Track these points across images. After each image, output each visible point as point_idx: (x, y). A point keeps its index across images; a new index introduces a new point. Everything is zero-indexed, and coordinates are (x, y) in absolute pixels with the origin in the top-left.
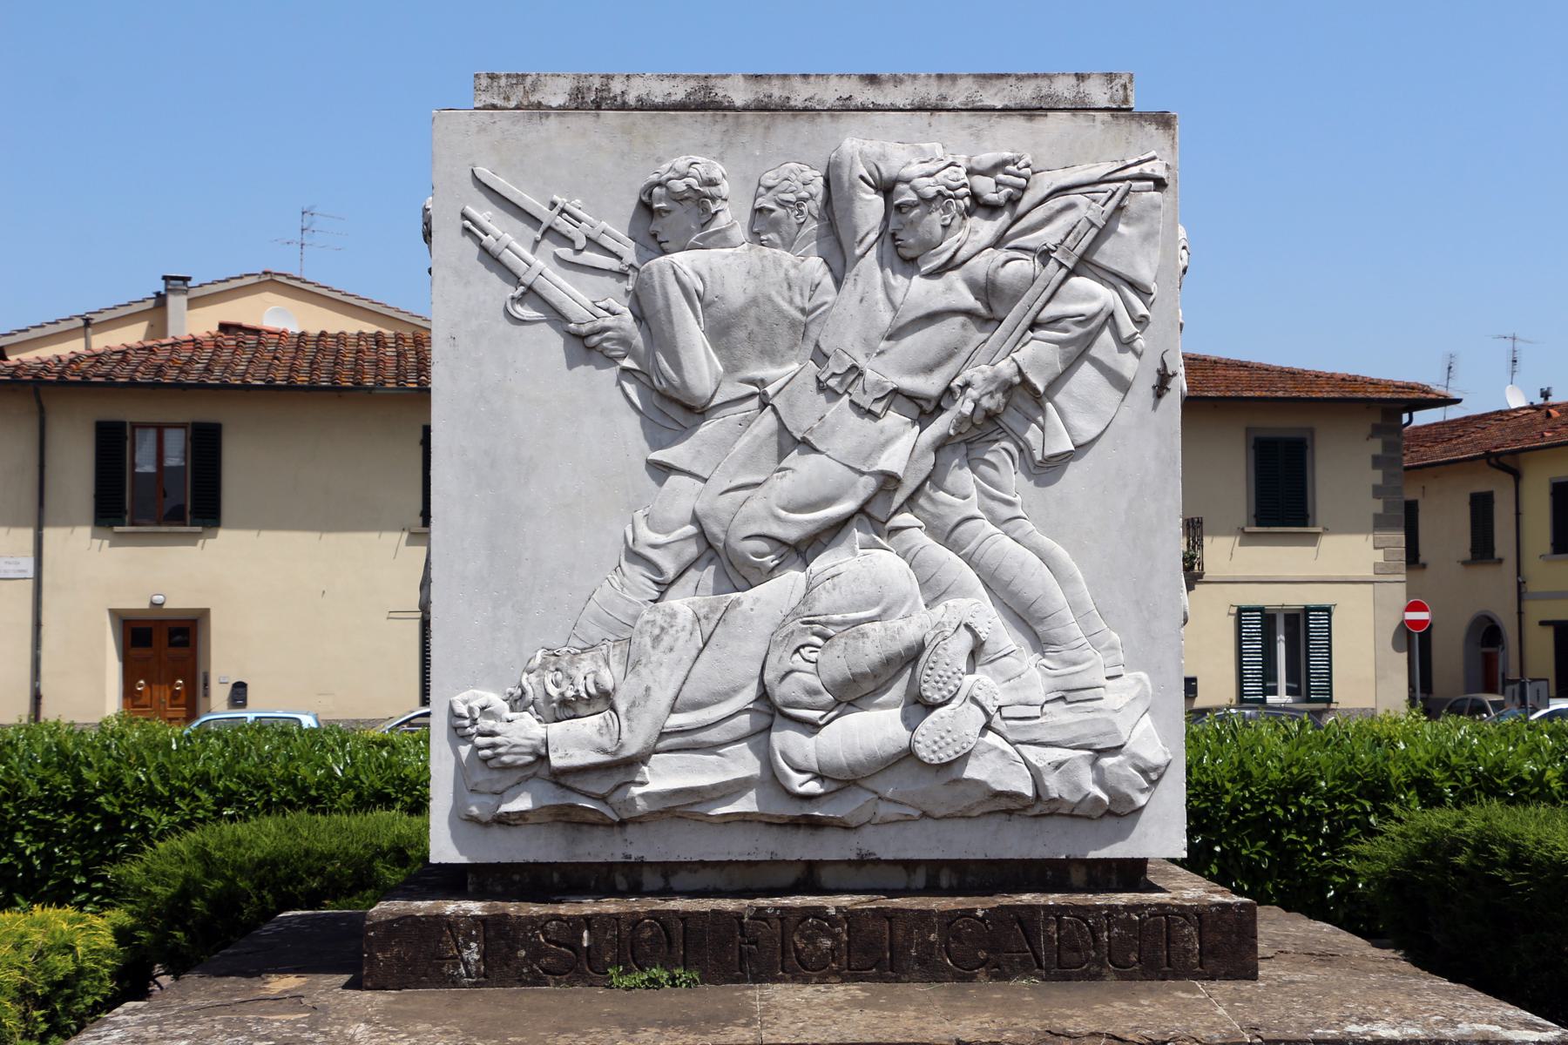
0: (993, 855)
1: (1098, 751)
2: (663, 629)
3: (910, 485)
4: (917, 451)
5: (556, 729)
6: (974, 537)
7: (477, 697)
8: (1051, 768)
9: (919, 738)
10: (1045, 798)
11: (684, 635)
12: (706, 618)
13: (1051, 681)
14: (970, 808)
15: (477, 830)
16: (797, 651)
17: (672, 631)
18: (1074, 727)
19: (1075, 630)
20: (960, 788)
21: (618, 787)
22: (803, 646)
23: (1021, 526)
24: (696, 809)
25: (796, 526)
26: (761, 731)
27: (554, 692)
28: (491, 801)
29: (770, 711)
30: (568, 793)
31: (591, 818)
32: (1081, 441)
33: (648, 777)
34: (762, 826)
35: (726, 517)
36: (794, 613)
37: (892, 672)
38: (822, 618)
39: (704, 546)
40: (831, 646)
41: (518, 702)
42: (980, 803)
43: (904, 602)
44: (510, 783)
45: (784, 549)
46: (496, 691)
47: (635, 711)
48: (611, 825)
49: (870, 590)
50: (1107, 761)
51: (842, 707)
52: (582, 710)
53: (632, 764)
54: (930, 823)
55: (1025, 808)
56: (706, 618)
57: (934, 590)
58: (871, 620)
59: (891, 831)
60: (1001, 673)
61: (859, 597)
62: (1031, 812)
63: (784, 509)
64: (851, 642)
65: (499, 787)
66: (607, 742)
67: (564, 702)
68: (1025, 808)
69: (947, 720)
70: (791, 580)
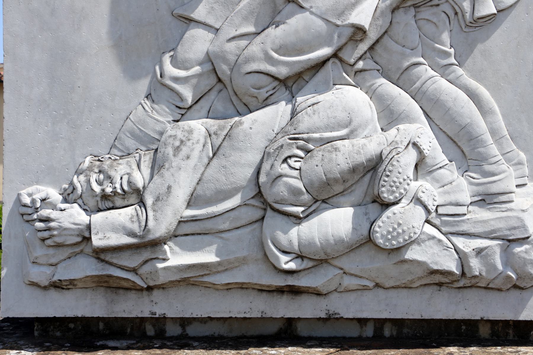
0: (426, 316)
1: (509, 241)
2: (182, 142)
3: (373, 36)
4: (378, 11)
5: (98, 218)
6: (419, 78)
7: (39, 191)
8: (474, 253)
9: (377, 229)
10: (468, 275)
11: (199, 147)
12: (216, 134)
13: (475, 188)
14: (412, 281)
15: (38, 292)
16: (285, 161)
17: (189, 143)
18: (492, 223)
19: (494, 150)
20: (406, 266)
21: (146, 262)
22: (290, 157)
23: (454, 71)
24: (206, 279)
25: (285, 65)
26: (256, 221)
27: (97, 189)
28: (48, 271)
29: (263, 203)
30: (107, 266)
31: (125, 284)
32: (502, 6)
33: (169, 254)
34: (255, 293)
35: (232, 58)
36: (283, 131)
37: (356, 178)
38: (305, 136)
39: (215, 80)
40: (311, 157)
41: (69, 196)
42: (419, 278)
43: (366, 126)
44: (62, 258)
45: (276, 83)
46: (54, 187)
47: (159, 204)
48: (141, 289)
49: (342, 116)
50: (518, 249)
51: (318, 204)
52: (119, 202)
53: (156, 244)
54: (381, 291)
55: (452, 282)
56: (216, 134)
57: (390, 117)
58: (342, 138)
59: (352, 297)
60: (437, 181)
61: (333, 121)
62: (456, 285)
63: (276, 52)
64: (326, 154)
65: (53, 261)
66: (135, 227)
67: (105, 197)
68: (452, 282)
69: (398, 215)
70: (281, 110)
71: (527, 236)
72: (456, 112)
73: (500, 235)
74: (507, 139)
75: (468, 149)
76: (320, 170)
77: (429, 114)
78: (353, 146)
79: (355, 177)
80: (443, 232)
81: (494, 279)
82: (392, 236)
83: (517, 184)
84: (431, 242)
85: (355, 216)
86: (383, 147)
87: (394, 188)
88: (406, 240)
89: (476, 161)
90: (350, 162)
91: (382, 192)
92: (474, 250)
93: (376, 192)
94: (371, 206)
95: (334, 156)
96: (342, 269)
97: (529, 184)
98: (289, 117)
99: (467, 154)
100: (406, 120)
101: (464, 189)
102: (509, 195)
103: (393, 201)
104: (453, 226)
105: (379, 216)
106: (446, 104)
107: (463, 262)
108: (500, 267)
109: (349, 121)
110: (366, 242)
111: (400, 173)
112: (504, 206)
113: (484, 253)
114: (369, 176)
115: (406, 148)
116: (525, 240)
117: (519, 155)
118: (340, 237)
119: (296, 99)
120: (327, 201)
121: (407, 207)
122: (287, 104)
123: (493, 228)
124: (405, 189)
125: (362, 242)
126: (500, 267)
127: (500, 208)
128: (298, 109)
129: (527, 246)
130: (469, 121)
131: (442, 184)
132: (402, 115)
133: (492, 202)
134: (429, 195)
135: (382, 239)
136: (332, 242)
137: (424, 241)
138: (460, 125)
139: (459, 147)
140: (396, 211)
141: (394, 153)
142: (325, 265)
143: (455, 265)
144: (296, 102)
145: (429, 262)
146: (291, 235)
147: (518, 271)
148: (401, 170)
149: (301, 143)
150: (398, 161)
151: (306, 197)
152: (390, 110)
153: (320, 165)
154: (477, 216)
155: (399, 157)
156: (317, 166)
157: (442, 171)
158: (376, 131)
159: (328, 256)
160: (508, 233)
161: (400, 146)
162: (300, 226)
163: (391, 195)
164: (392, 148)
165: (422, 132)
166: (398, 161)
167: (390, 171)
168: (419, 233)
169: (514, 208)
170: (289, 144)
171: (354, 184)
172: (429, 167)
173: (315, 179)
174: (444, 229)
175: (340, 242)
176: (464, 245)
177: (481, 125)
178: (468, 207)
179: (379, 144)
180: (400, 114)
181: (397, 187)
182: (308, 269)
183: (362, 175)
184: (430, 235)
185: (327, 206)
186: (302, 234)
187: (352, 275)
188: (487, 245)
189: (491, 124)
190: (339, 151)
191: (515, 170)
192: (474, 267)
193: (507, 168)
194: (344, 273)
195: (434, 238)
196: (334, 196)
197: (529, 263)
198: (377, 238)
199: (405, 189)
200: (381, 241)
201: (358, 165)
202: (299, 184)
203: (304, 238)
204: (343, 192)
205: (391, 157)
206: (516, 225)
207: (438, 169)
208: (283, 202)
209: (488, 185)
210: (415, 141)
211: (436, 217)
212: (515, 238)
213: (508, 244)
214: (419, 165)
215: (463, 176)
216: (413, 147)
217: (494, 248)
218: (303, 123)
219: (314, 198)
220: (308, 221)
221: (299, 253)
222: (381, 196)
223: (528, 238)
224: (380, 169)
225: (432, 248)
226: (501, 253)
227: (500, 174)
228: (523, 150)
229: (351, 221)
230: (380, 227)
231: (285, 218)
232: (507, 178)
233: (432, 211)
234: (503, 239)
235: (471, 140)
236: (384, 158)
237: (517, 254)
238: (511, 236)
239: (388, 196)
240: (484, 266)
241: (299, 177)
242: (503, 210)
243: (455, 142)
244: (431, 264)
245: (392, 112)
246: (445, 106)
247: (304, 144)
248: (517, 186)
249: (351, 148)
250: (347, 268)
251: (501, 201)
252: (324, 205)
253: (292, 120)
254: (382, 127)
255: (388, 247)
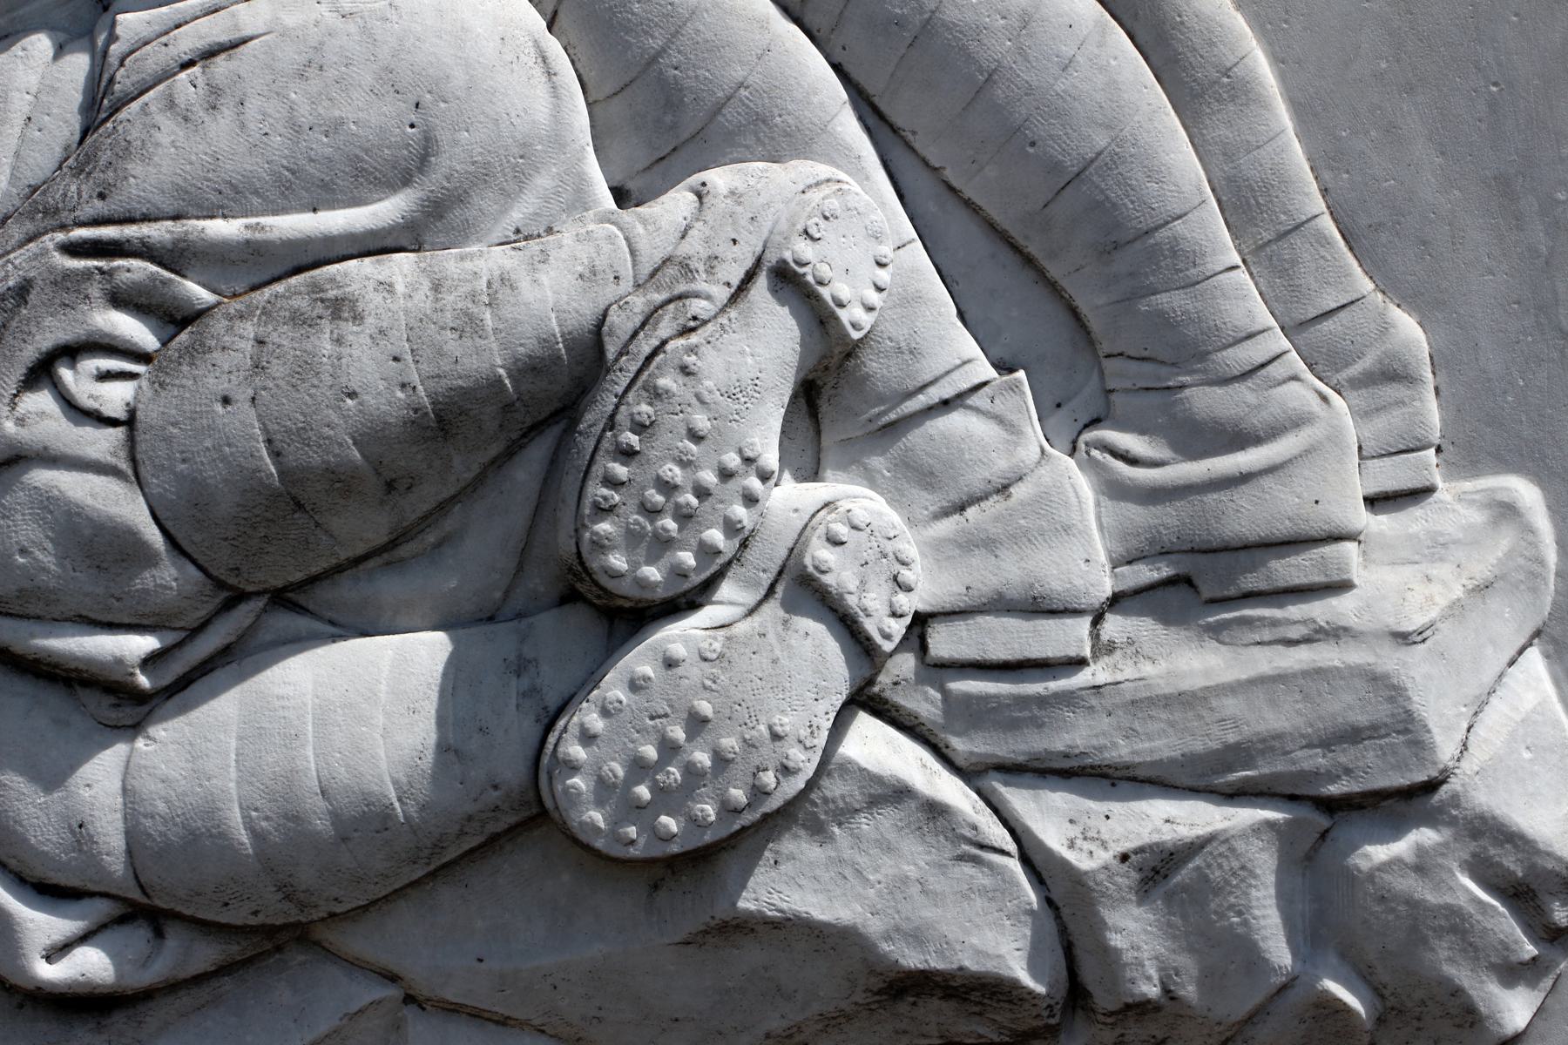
1: (1330, 806)
8: (1127, 878)
9: (577, 751)
10: (1103, 1000)
13: (1136, 514)
16: (41, 373)
19: (1244, 299)
20: (750, 956)
22: (72, 352)
36: (40, 207)
37: (464, 466)
40: (196, 352)
43: (522, 177)
49: (373, 117)
51: (243, 615)
58: (375, 245)
60: (926, 478)
61: (321, 145)
64: (282, 336)
69: (693, 672)
71: (1421, 777)
72: (1030, 90)
73: (1276, 776)
74: (1323, 240)
75: (1101, 300)
76: (243, 424)
77: (883, 107)
78: (436, 287)
79: (457, 461)
80: (960, 761)
81: (1250, 1019)
82: (656, 789)
83: (1374, 488)
84: (886, 820)
85: (457, 678)
86: (610, 292)
87: (669, 524)
88: (737, 811)
89: (1147, 367)
90: (415, 379)
91: (600, 545)
92: (1124, 858)
93: (566, 546)
94: (546, 622)
95: (327, 347)
96: (393, 978)
97: (1446, 491)
98: (76, 123)
99: (1095, 324)
100: (750, 140)
101: (1074, 519)
102: (1328, 550)
103: (661, 594)
104: (1014, 725)
105: (592, 678)
106: (973, 46)
107: (1071, 927)
108: (1280, 953)
109: (416, 148)
110: (512, 831)
111: (696, 437)
112: (1295, 611)
113: (1183, 875)
114: (537, 453)
115: (734, 298)
116: (1417, 803)
117: (1385, 328)
118: (367, 798)
119: (113, 24)
120: (301, 599)
121: (742, 628)
122: (60, 51)
123: (1232, 738)
124: (731, 528)
125: (500, 826)
126: (1280, 953)
127: (1274, 623)
128: (124, 80)
129: (1426, 836)
130: (1101, 140)
131: (954, 496)
132: (731, 114)
133: (1232, 591)
134: (869, 555)
135: (599, 803)
136: (321, 824)
137: (845, 814)
138: (1055, 167)
139: (1054, 288)
140: (678, 650)
141: (665, 328)
142: (297, 957)
143: (1025, 944)
144: (112, 38)
145: (874, 926)
146: (86, 793)
147: (1383, 976)
148: (701, 421)
149: (137, 269)
150: (685, 370)
151: (167, 577)
152: (661, 80)
153: (242, 395)
154: (1147, 669)
155: (692, 350)
156: (226, 401)
157: (955, 421)
158: (579, 201)
159: (302, 906)
160: (1318, 760)
161: (700, 286)
162: (140, 743)
163: (650, 561)
164: (659, 297)
165: (834, 204)
166: (685, 370)
167: (640, 428)
168: (809, 770)
169: (1352, 621)
170: (67, 281)
171: (453, 499)
172: (881, 399)
173: (213, 474)
174: (960, 745)
175: (364, 823)
176: (1074, 831)
177: (1177, 159)
178: (1098, 620)
179: (590, 275)
180: (718, 109)
181: (685, 517)
182: (199, 979)
183: (494, 450)
184: (877, 779)
185: (302, 623)
186: (148, 786)
187: (452, 1009)
188: (1200, 831)
189: (1229, 156)
190: (358, 318)
191: (1361, 415)
192: (1128, 957)
193: (1315, 404)
194: (409, 999)
195: (898, 793)
196: (338, 569)
197: (1440, 932)
198: (574, 797)
199: (731, 528)
200: (597, 817)
201: (464, 392)
202: (126, 506)
203: (161, 807)
204: (393, 544)
205: (646, 350)
206: (1361, 719)
207: (946, 405)
208: (32, 609)
209: (1211, 498)
210: (788, 256)
211: (921, 679)
212: (1355, 787)
213: (1323, 821)
214: (827, 392)
215: (1072, 452)
216: (774, 291)
217: (1240, 846)
218: (146, 159)
219: (220, 584)
220: (184, 709)
221: (136, 895)
222: (594, 565)
223: (1431, 786)
224: (589, 417)
225: (888, 848)
226: (1281, 872)
227: (1273, 432)
228: (1410, 300)
229: (430, 706)
230: (587, 738)
231: (54, 698)
232: (1319, 450)
233: (888, 646)
234: (1293, 798)
235: (1117, 246)
236: (611, 351)
237: (1371, 876)
238: (1334, 778)
239: (635, 566)
240: (1191, 950)
241: (124, 466)
242: (1294, 633)
243: (1029, 261)
244: (888, 938)
245: (670, 97)
246: (969, 58)
247: (153, 277)
248: (1374, 502)
249: (423, 299)
250: (419, 968)
251: (1281, 584)
252: (285, 622)
253: (89, 140)
254: (618, 179)
255: (633, 852)
